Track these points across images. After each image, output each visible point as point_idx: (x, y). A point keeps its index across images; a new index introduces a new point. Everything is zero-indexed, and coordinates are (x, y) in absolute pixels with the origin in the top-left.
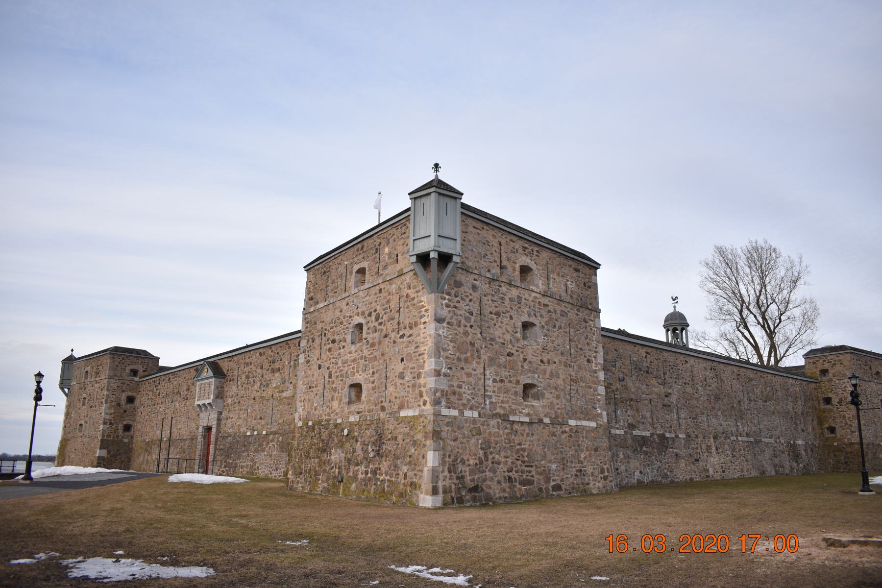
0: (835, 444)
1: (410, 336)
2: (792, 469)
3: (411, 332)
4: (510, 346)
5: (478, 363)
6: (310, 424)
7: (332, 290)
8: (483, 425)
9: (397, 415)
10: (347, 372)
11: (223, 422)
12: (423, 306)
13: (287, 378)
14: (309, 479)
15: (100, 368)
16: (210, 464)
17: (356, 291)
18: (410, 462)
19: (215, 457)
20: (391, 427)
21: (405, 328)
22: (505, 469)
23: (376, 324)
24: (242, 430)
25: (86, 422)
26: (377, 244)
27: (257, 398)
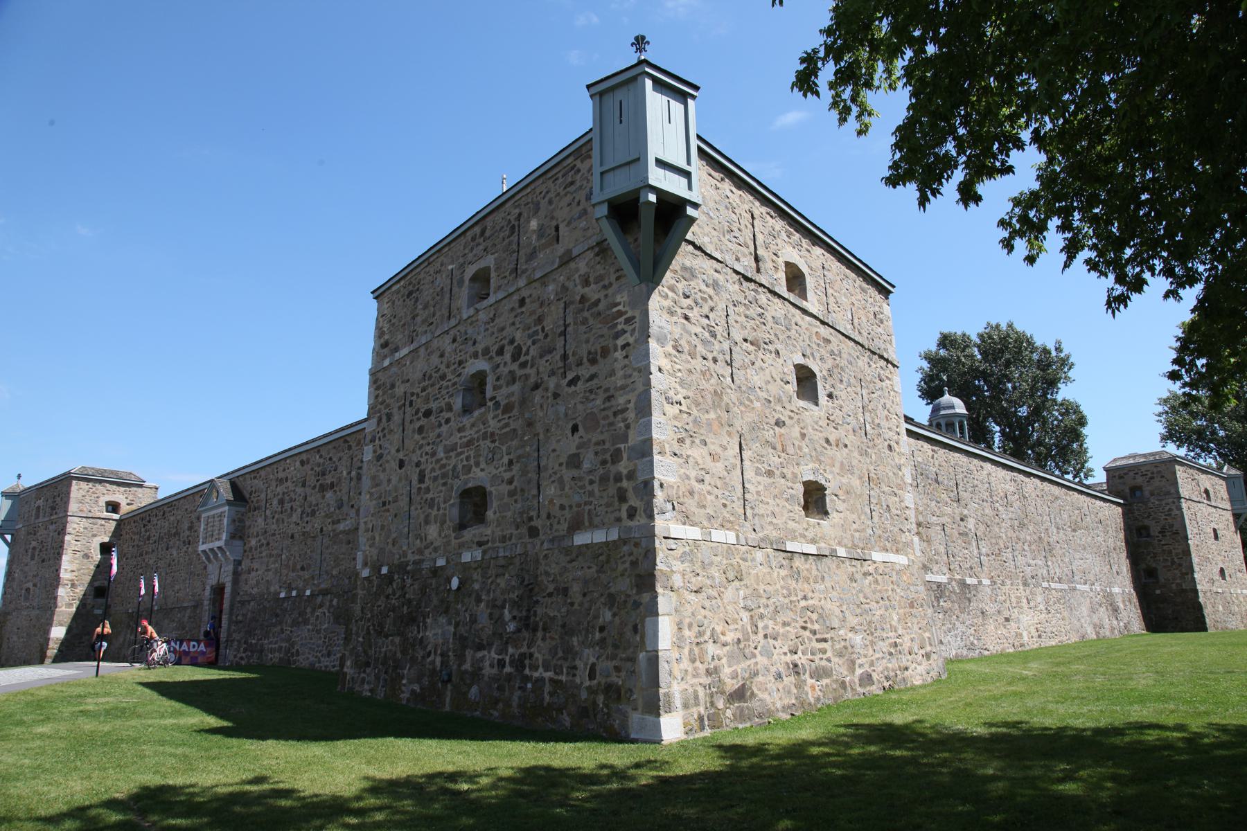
0: (1158, 592)
1: (592, 377)
2: (1112, 629)
3: (593, 370)
4: (779, 408)
5: (729, 434)
6: (384, 570)
7: (424, 322)
8: (745, 560)
9: (566, 543)
10: (455, 467)
11: (243, 577)
12: (620, 314)
13: (345, 498)
14: (383, 676)
15: (58, 499)
16: (222, 646)
17: (472, 311)
18: (603, 640)
19: (229, 635)
20: (554, 569)
21: (580, 364)
22: (785, 649)
23: (515, 367)
24: (272, 589)
25: (35, 585)
26: (512, 218)
27: (296, 536)
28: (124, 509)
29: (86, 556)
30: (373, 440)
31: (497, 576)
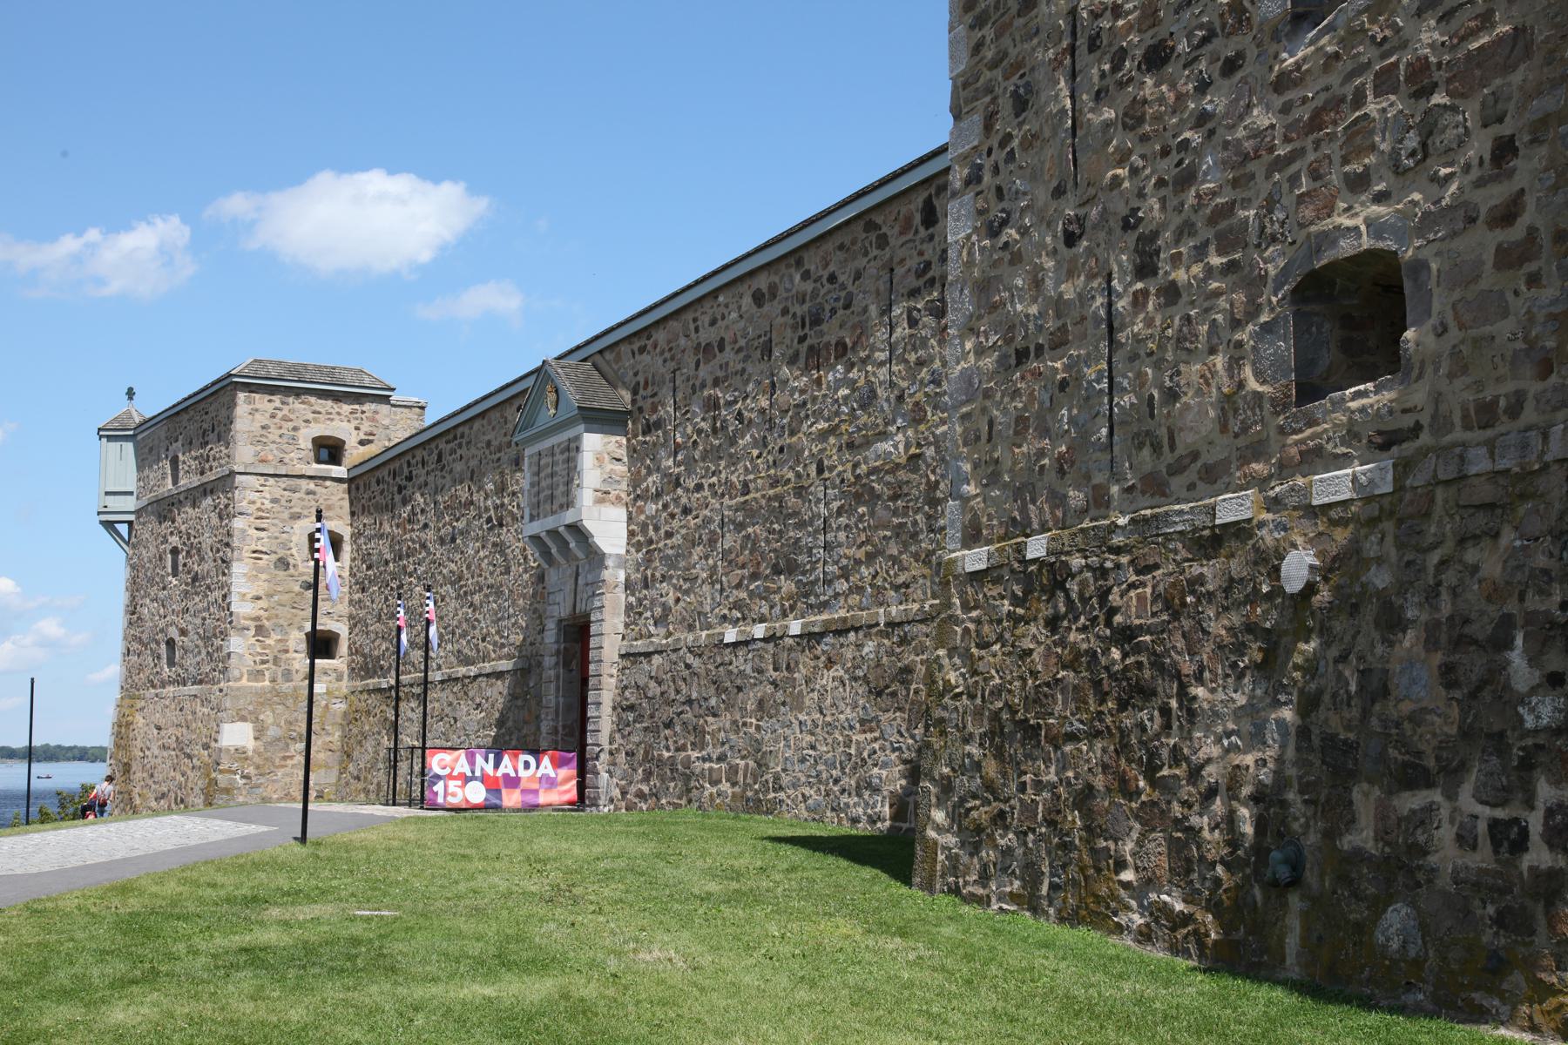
28: (355, 453)
29: (283, 564)
30: (974, 179)
31: (1462, 541)
